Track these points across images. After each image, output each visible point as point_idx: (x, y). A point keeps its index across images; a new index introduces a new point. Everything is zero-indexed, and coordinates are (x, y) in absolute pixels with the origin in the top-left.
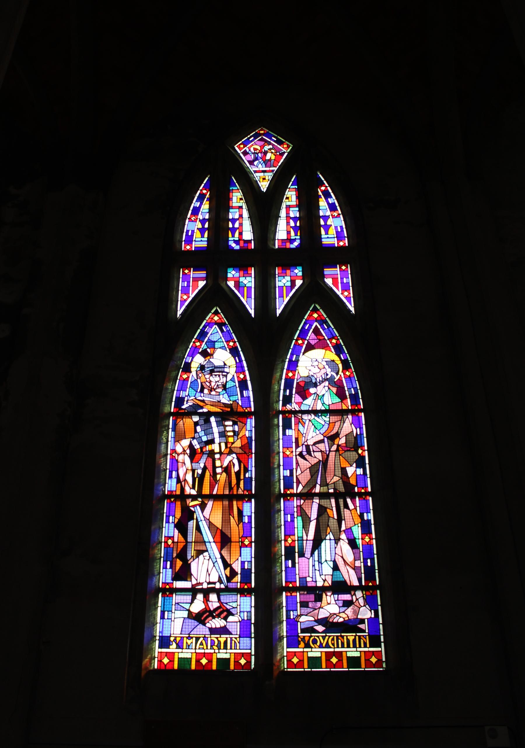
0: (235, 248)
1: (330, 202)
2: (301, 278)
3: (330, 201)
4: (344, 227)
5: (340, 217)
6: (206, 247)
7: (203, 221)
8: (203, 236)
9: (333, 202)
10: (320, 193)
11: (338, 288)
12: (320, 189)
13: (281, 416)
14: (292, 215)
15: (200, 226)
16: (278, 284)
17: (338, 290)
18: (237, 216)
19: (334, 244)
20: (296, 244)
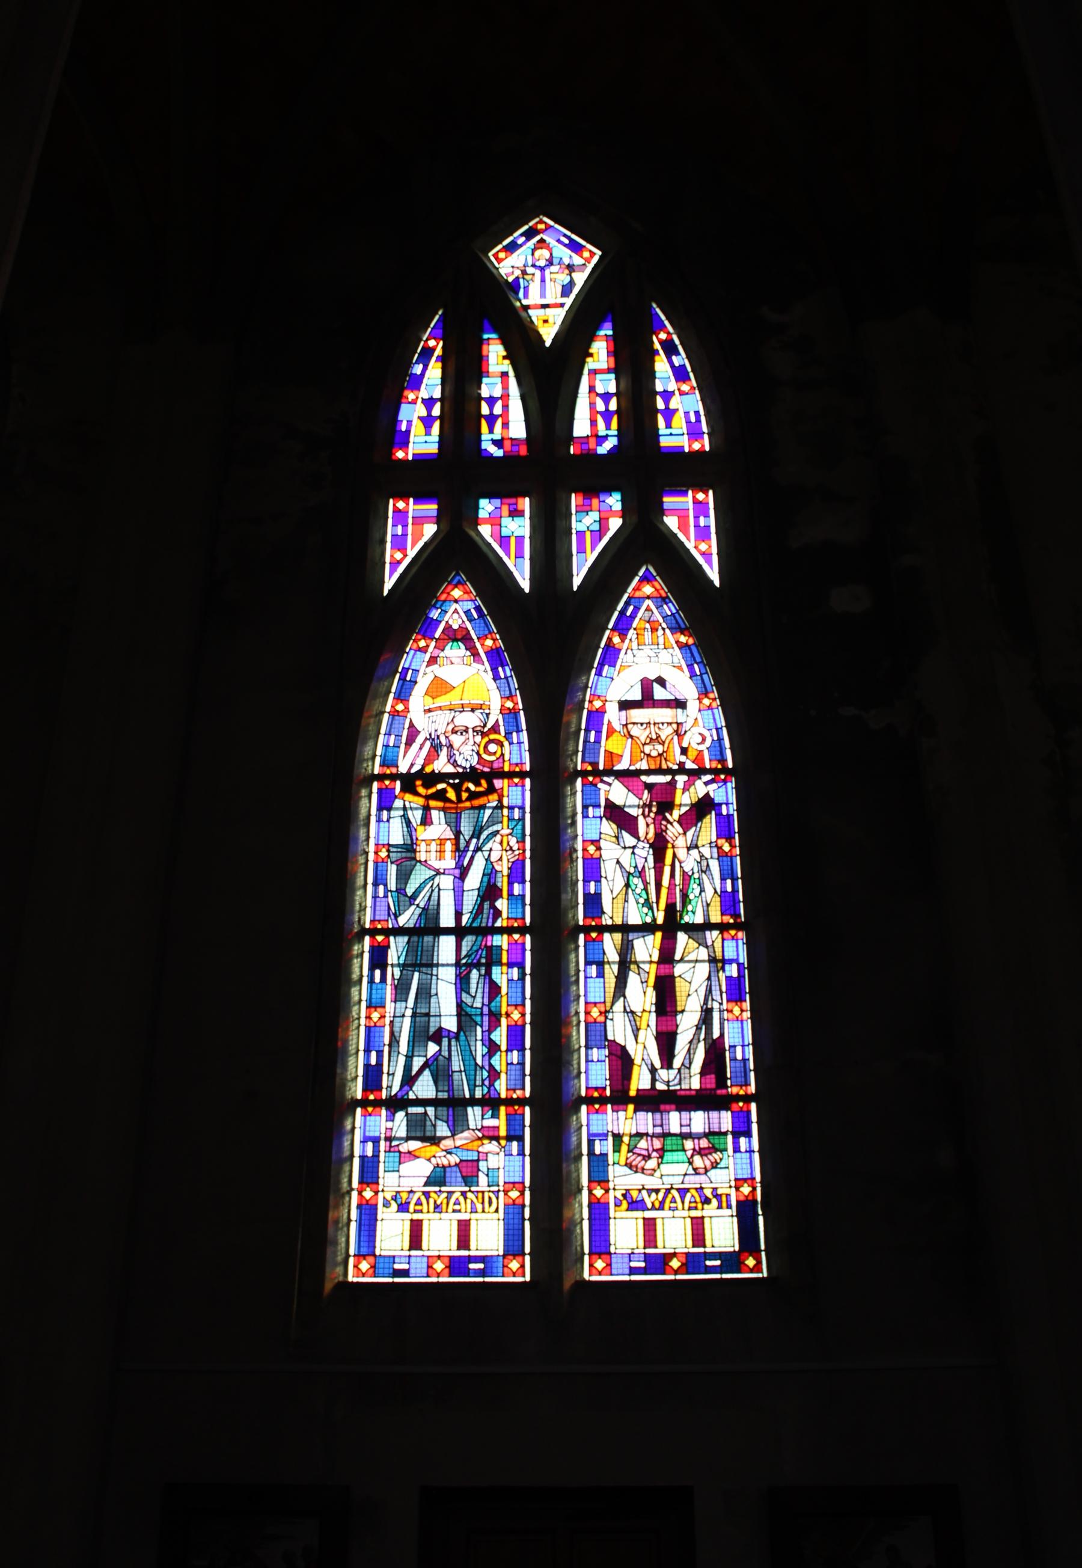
0: (494, 455)
1: (677, 364)
2: (620, 514)
3: (677, 361)
4: (702, 412)
5: (695, 393)
6: (401, 783)
7: (429, 403)
8: (428, 433)
9: (682, 363)
10: (657, 346)
12: (657, 337)
13: (582, 937)
14: (600, 389)
15: (423, 412)
16: (576, 526)
17: (688, 539)
18: (497, 392)
19: (683, 447)
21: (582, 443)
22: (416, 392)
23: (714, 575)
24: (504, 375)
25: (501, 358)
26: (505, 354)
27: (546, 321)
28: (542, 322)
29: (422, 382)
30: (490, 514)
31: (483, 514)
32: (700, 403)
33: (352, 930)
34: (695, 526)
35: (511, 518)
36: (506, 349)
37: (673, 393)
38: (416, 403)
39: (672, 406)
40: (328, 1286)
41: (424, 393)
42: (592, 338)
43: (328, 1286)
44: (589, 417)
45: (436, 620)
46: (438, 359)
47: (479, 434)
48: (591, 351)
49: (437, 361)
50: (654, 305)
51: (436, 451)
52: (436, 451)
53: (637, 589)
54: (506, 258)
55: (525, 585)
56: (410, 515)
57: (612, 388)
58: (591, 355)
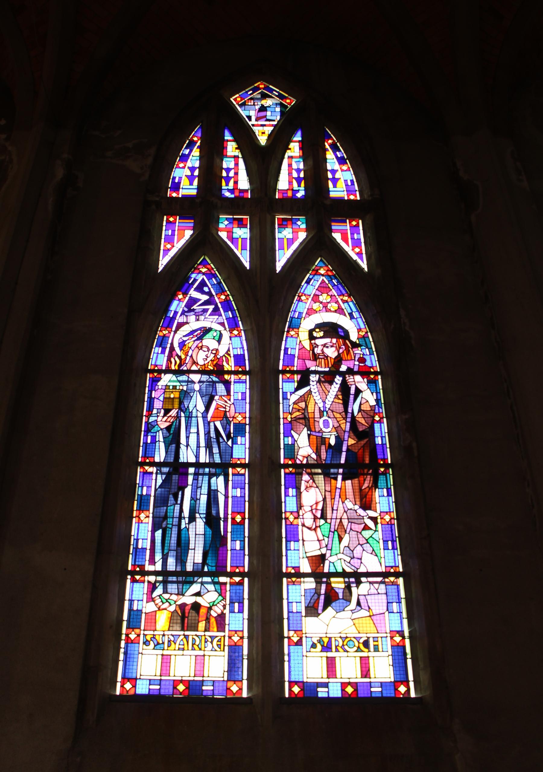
4: (355, 180)
7: (192, 169)
8: (191, 184)
10: (327, 146)
11: (347, 243)
15: (189, 173)
16: (278, 235)
20: (299, 195)
21: (283, 193)
22: (185, 163)
24: (236, 158)
26: (237, 146)
32: (353, 176)
34: (351, 239)
35: (239, 229)
37: (337, 170)
41: (189, 164)
42: (290, 141)
44: (288, 180)
46: (198, 147)
48: (290, 147)
49: (197, 148)
51: (195, 194)
52: (195, 194)
55: (247, 265)
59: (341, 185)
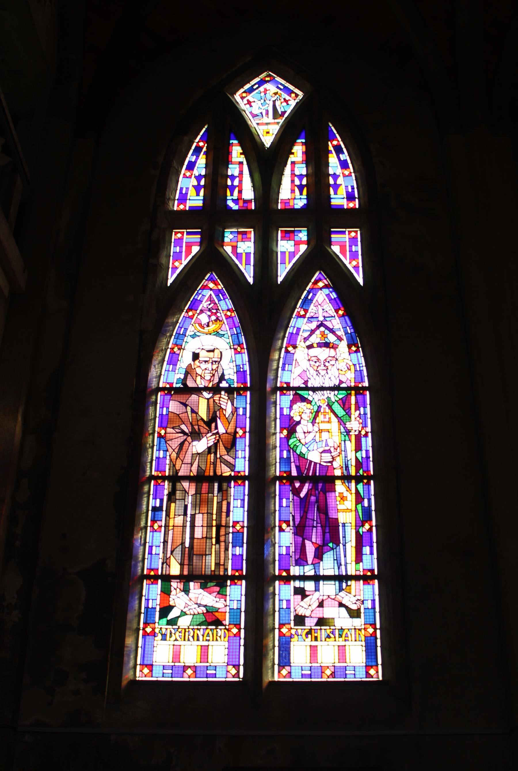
1: (342, 159)
3: (342, 157)
4: (355, 186)
7: (198, 178)
8: (198, 194)
9: (345, 159)
10: (331, 148)
12: (331, 143)
14: (297, 172)
15: (196, 183)
19: (343, 205)
22: (191, 172)
23: (360, 280)
24: (241, 163)
25: (239, 154)
26: (242, 151)
27: (268, 133)
28: (266, 133)
29: (195, 166)
30: (231, 240)
31: (226, 240)
33: (144, 475)
36: (242, 149)
37: (339, 176)
38: (191, 178)
39: (338, 182)
40: (124, 683)
41: (196, 172)
43: (124, 683)
45: (199, 300)
47: (226, 196)
48: (293, 151)
50: (331, 125)
51: (202, 205)
52: (202, 205)
53: (316, 282)
54: (247, 96)
55: (251, 280)
56: (184, 241)
57: (304, 173)
58: (293, 153)
59: (342, 192)
